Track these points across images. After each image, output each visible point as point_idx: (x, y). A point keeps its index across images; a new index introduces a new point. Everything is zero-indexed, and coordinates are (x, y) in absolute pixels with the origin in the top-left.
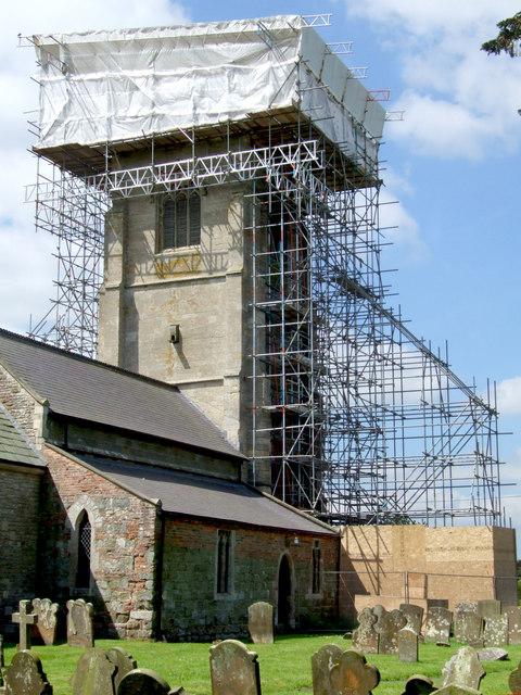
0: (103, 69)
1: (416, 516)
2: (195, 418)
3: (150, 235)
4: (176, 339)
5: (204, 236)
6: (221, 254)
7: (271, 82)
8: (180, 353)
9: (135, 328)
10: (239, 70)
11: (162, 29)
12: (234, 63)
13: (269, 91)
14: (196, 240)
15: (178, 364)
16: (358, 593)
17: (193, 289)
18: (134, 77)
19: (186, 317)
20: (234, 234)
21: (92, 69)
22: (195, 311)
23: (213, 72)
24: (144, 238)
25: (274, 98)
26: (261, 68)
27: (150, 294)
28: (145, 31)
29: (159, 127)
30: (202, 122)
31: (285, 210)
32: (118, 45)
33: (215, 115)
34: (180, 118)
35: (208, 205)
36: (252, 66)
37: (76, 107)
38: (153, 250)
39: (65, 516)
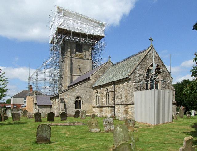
0: (71, 17)
2: (40, 90)
3: (75, 49)
4: (80, 68)
5: (84, 52)
8: (80, 70)
9: (72, 65)
13: (99, 32)
14: (82, 52)
15: (79, 72)
17: (82, 60)
19: (81, 64)
21: (68, 16)
22: (83, 64)
25: (101, 34)
26: (99, 28)
27: (75, 59)
30: (89, 33)
34: (86, 31)
39: (167, 65)
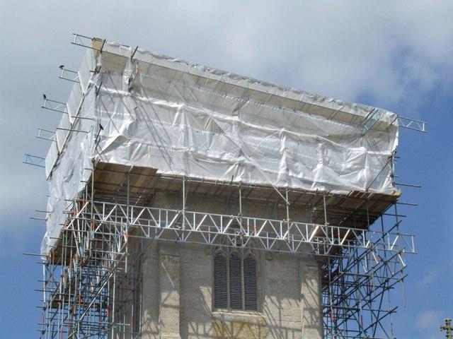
1: (204, 331)
3: (207, 293)
6: (294, 330)
7: (367, 167)
10: (331, 145)
11: (253, 81)
12: (330, 137)
16: (154, 321)
18: (219, 120)
20: (311, 310)
23: (303, 139)
24: (201, 295)
25: (373, 182)
28: (232, 76)
29: (246, 177)
31: (186, 222)
32: (199, 80)
33: (310, 183)
34: (277, 175)
35: (271, 272)
36: (344, 146)
37: (143, 125)
38: (210, 305)
